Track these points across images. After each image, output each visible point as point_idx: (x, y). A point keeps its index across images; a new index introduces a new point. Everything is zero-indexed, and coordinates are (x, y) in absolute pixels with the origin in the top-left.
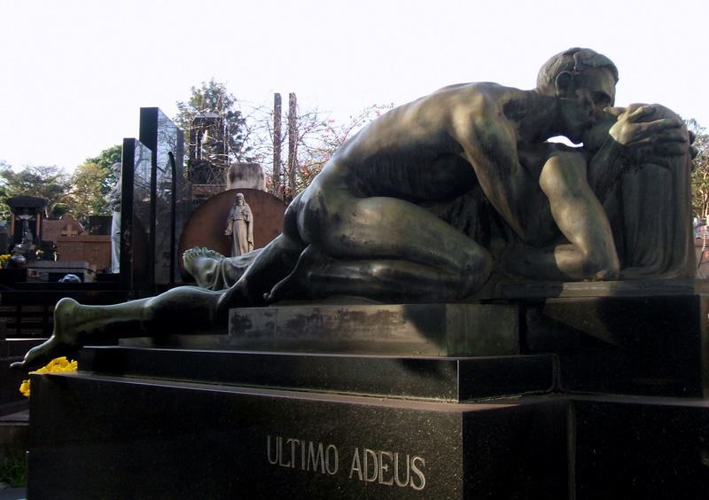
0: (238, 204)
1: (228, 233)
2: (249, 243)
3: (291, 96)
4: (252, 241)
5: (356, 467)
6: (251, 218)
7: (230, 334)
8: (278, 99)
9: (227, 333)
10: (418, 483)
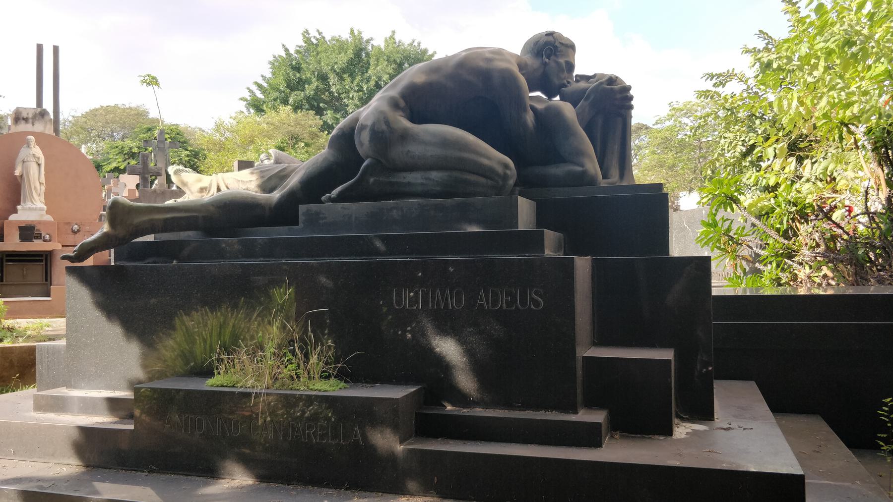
0: (29, 146)
1: (17, 173)
2: (40, 184)
3: (56, 50)
4: (44, 182)
5: (481, 300)
6: (42, 161)
7: (301, 225)
8: (40, 48)
9: (297, 224)
10: (537, 304)
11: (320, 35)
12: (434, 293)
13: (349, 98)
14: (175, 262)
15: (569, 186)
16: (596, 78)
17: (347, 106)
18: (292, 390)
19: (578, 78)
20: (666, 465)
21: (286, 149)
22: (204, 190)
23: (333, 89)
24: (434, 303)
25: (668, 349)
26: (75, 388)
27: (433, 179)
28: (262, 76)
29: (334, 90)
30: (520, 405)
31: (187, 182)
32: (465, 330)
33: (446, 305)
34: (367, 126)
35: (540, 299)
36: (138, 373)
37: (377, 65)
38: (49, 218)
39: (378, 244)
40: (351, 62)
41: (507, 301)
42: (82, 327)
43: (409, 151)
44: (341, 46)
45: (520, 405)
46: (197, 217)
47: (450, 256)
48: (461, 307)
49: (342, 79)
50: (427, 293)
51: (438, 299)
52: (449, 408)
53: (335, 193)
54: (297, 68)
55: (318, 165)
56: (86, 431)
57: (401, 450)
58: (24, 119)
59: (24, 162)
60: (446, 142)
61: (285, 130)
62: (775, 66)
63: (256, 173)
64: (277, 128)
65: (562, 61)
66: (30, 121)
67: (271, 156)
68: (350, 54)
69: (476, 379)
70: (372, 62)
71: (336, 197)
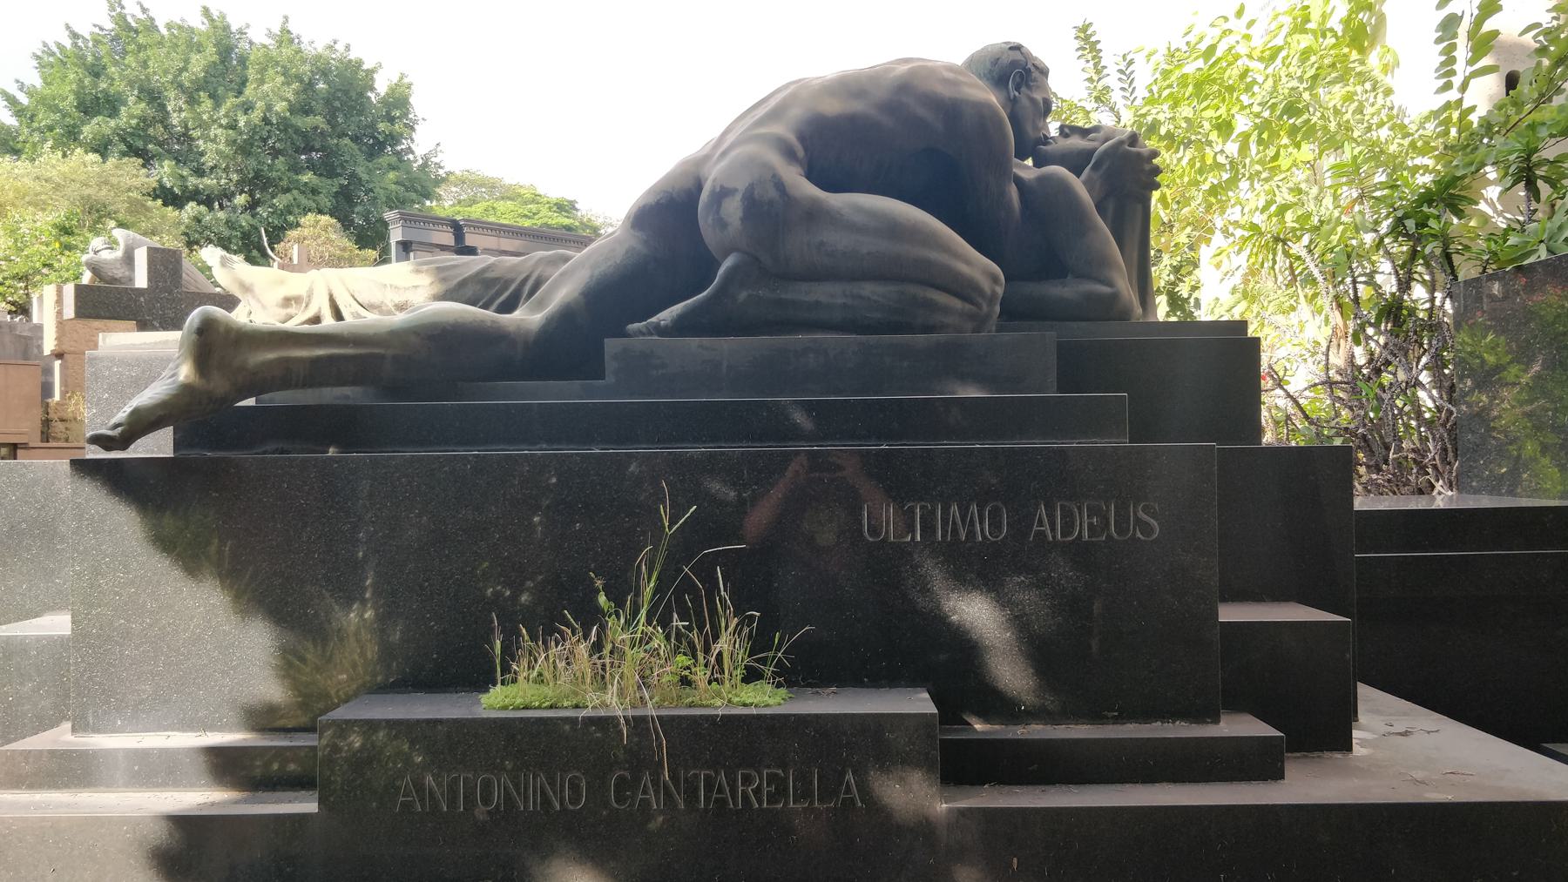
5: (1041, 523)
11: (144, 13)
12: (946, 511)
13: (207, 139)
14: (332, 452)
15: (1088, 320)
16: (1102, 133)
17: (202, 154)
18: (690, 706)
19: (1067, 130)
20: (1423, 801)
21: (76, 231)
22: (293, 302)
23: (175, 119)
24: (947, 532)
25: (1283, 604)
26: (97, 730)
27: (869, 298)
28: (17, 81)
29: (175, 122)
30: (1116, 714)
31: (252, 285)
32: (1008, 579)
33: (971, 534)
34: (736, 190)
35: (1152, 520)
36: (271, 690)
37: (262, 82)
39: (799, 417)
40: (210, 70)
41: (1091, 525)
42: (117, 594)
43: (822, 244)
44: (186, 41)
45: (1116, 714)
46: (383, 357)
47: (945, 442)
48: (1001, 537)
49: (192, 101)
50: (933, 512)
51: (954, 523)
52: (978, 727)
53: (666, 316)
54: (96, 72)
55: (618, 262)
56: (183, 823)
57: (944, 812)
60: (894, 229)
61: (76, 193)
62: (1163, 131)
63: (427, 271)
64: (58, 187)
65: (1038, 96)
67: (117, 244)
68: (211, 53)
69: (1031, 670)
70: (252, 73)
71: (670, 325)
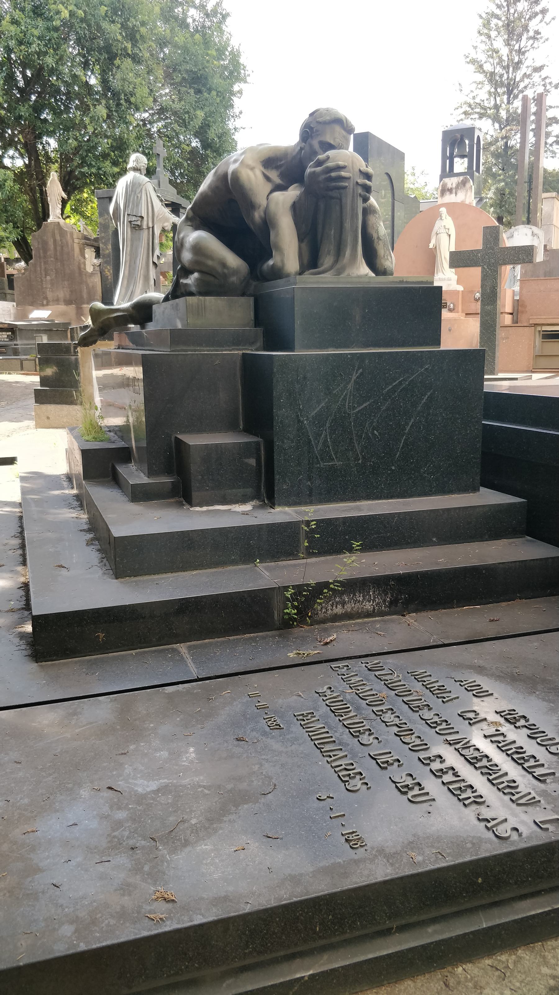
6: (453, 232)
38: (460, 288)
58: (448, 190)
59: (437, 234)
66: (454, 191)
